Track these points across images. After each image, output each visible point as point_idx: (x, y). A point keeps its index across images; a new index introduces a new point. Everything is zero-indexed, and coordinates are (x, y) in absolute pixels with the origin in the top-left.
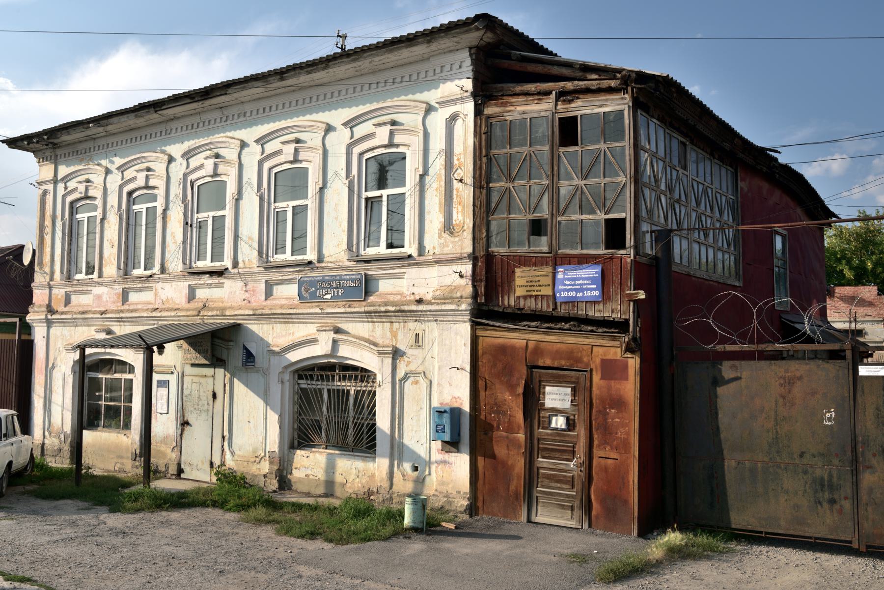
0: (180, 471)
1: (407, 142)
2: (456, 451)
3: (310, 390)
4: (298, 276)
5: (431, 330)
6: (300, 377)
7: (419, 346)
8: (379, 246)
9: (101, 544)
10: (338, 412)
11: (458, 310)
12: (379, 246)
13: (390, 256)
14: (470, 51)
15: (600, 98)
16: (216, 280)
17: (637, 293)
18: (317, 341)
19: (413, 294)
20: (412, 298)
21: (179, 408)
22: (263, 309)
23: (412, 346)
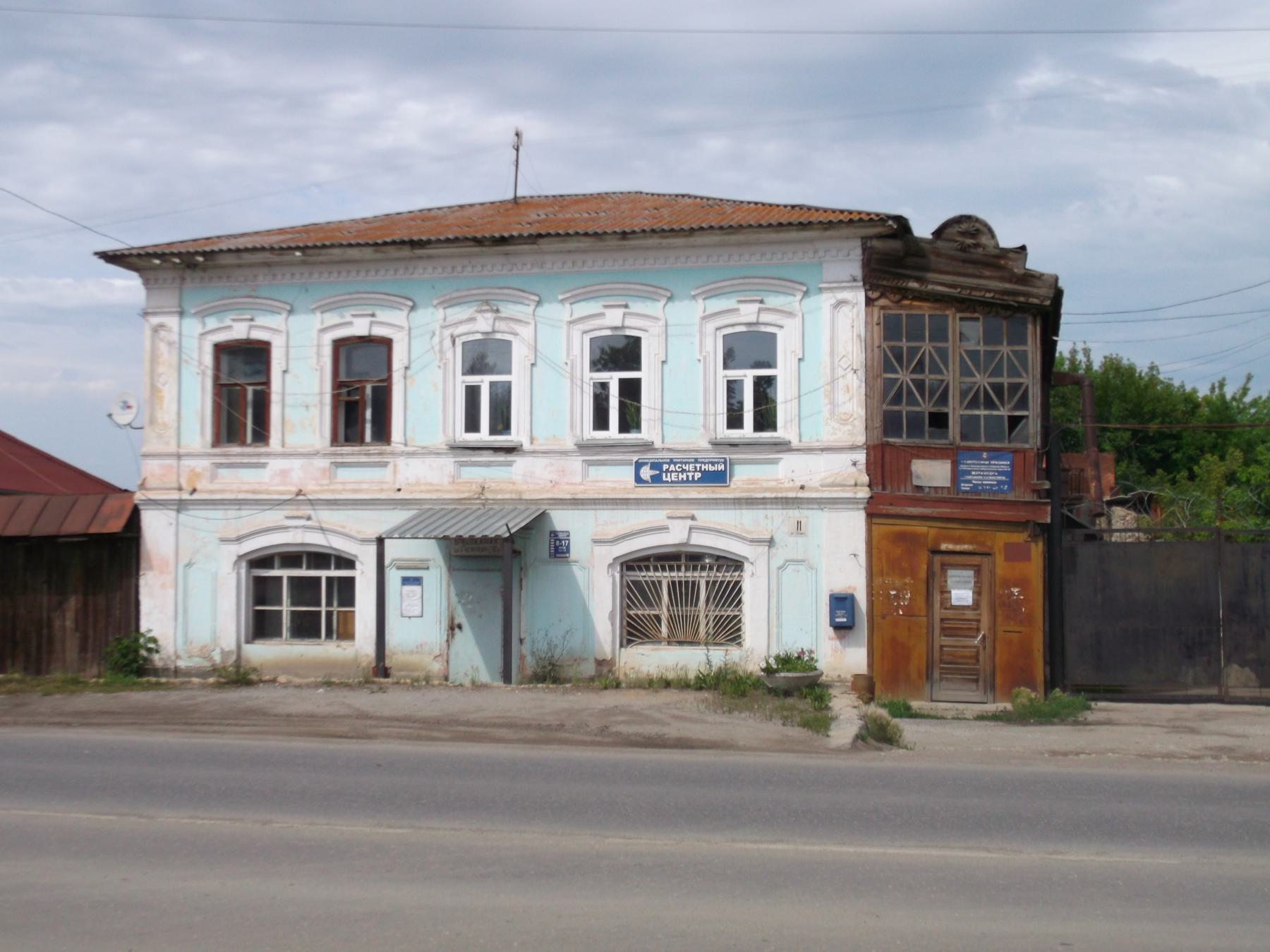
0: (446, 679)
1: (780, 323)
2: (1024, 421)
3: (646, 582)
4: (635, 459)
5: (818, 520)
6: (630, 568)
7: (801, 534)
8: (490, 382)
9: (1101, 418)
10: (682, 606)
11: (855, 498)
12: (490, 382)
13: (770, 440)
14: (862, 241)
15: (972, 528)
16: (501, 458)
17: (1041, 484)
18: (668, 528)
19: (793, 480)
20: (791, 484)
21: (443, 608)
22: (585, 493)
23: (792, 534)
